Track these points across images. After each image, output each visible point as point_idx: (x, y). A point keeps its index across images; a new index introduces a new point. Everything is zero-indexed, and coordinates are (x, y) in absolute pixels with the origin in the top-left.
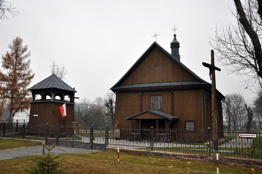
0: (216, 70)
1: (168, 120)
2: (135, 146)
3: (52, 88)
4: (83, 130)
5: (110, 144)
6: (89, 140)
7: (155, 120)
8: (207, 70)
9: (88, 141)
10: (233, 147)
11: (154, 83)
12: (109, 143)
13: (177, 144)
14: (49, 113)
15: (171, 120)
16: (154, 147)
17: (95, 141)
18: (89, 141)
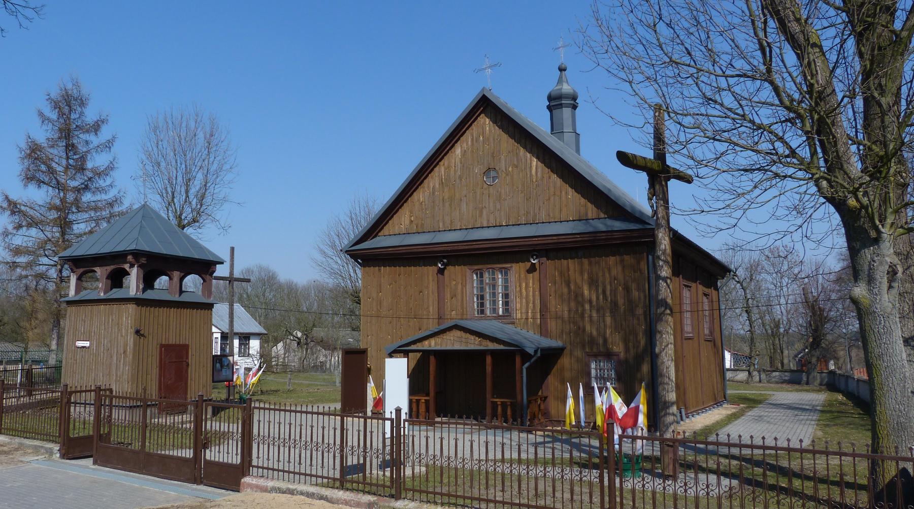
0: (672, 180)
1: (525, 356)
2: (317, 476)
3: (69, 260)
4: (468, 437)
5: (258, 467)
6: (237, 454)
7: (481, 354)
8: (642, 178)
9: (234, 456)
10: (524, 456)
11: (483, 227)
12: (253, 464)
13: (174, 414)
14: (122, 336)
15: (535, 355)
16: (404, 485)
17: (211, 451)
18: (239, 457)
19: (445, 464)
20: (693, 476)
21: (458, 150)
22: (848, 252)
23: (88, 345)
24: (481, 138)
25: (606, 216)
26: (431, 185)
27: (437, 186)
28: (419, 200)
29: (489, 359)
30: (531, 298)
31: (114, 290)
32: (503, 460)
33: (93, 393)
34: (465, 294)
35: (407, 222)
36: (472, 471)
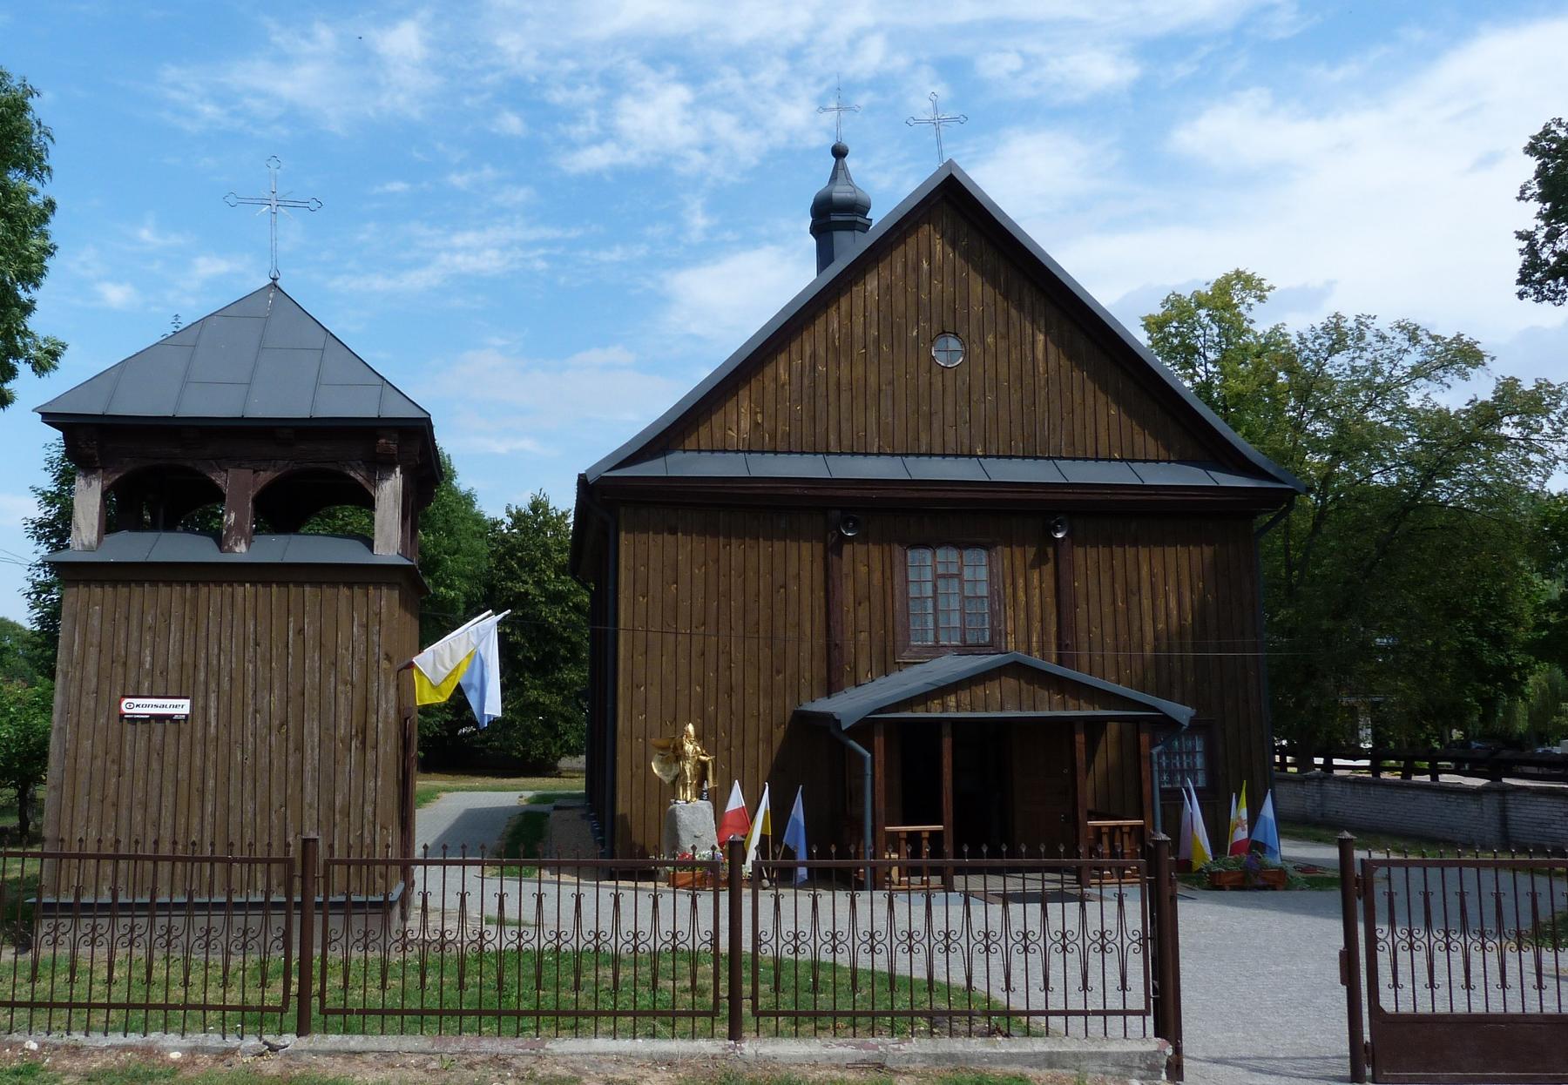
21: (872, 283)
22: (1002, 552)
23: (186, 710)
24: (925, 265)
26: (808, 351)
27: (821, 352)
28: (776, 379)
29: (947, 730)
30: (1037, 610)
31: (124, 535)
32: (501, 922)
33: (581, 881)
35: (745, 424)
36: (778, 963)
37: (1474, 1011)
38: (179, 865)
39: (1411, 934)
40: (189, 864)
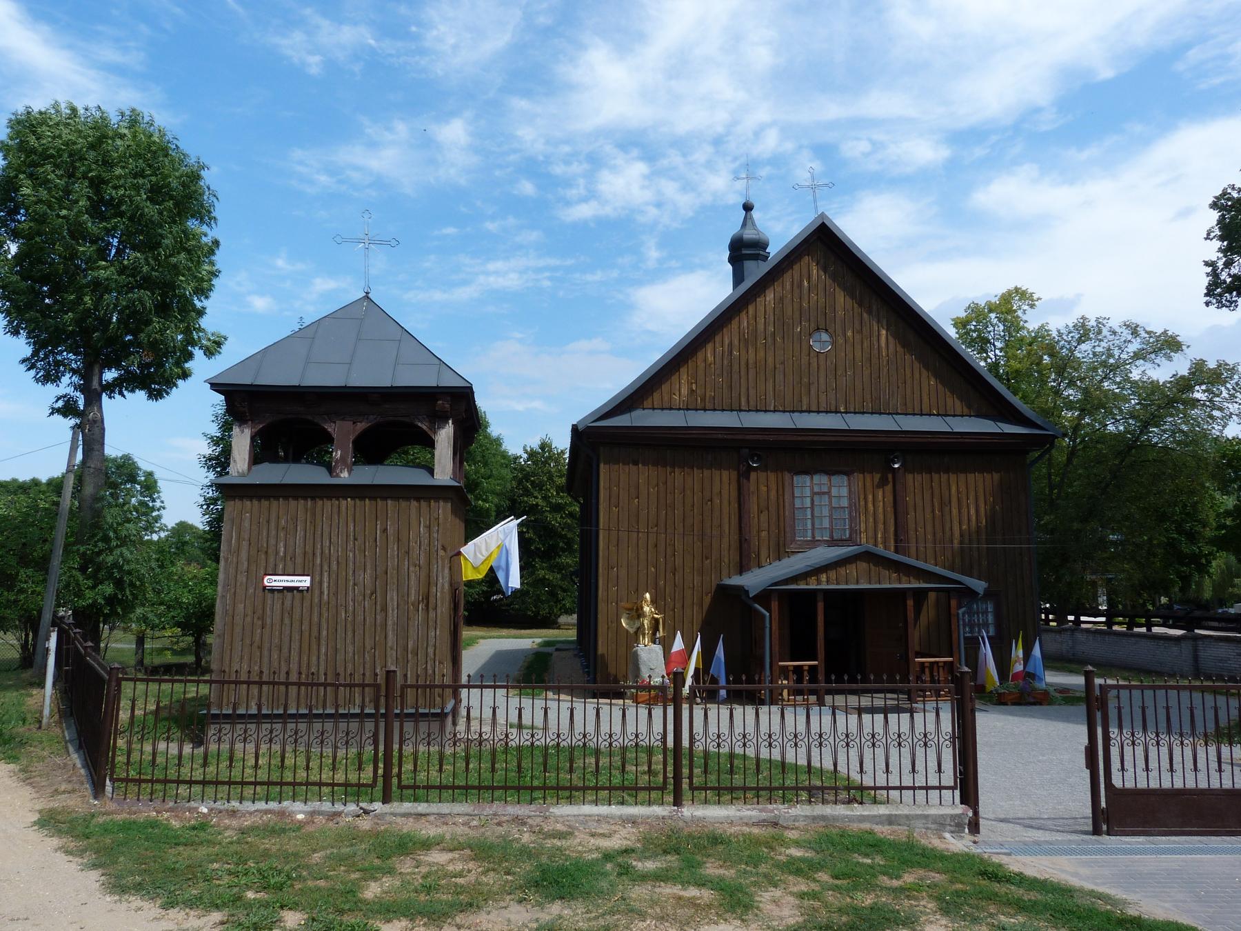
19: (1164, 738)
20: (357, 725)
21: (770, 296)
24: (806, 283)
25: (1156, 435)
26: (727, 342)
27: (736, 342)
30: (881, 516)
32: (520, 726)
34: (782, 507)
35: (684, 391)
37: (1175, 787)
38: (303, 688)
39: (1133, 735)
40: (310, 688)
